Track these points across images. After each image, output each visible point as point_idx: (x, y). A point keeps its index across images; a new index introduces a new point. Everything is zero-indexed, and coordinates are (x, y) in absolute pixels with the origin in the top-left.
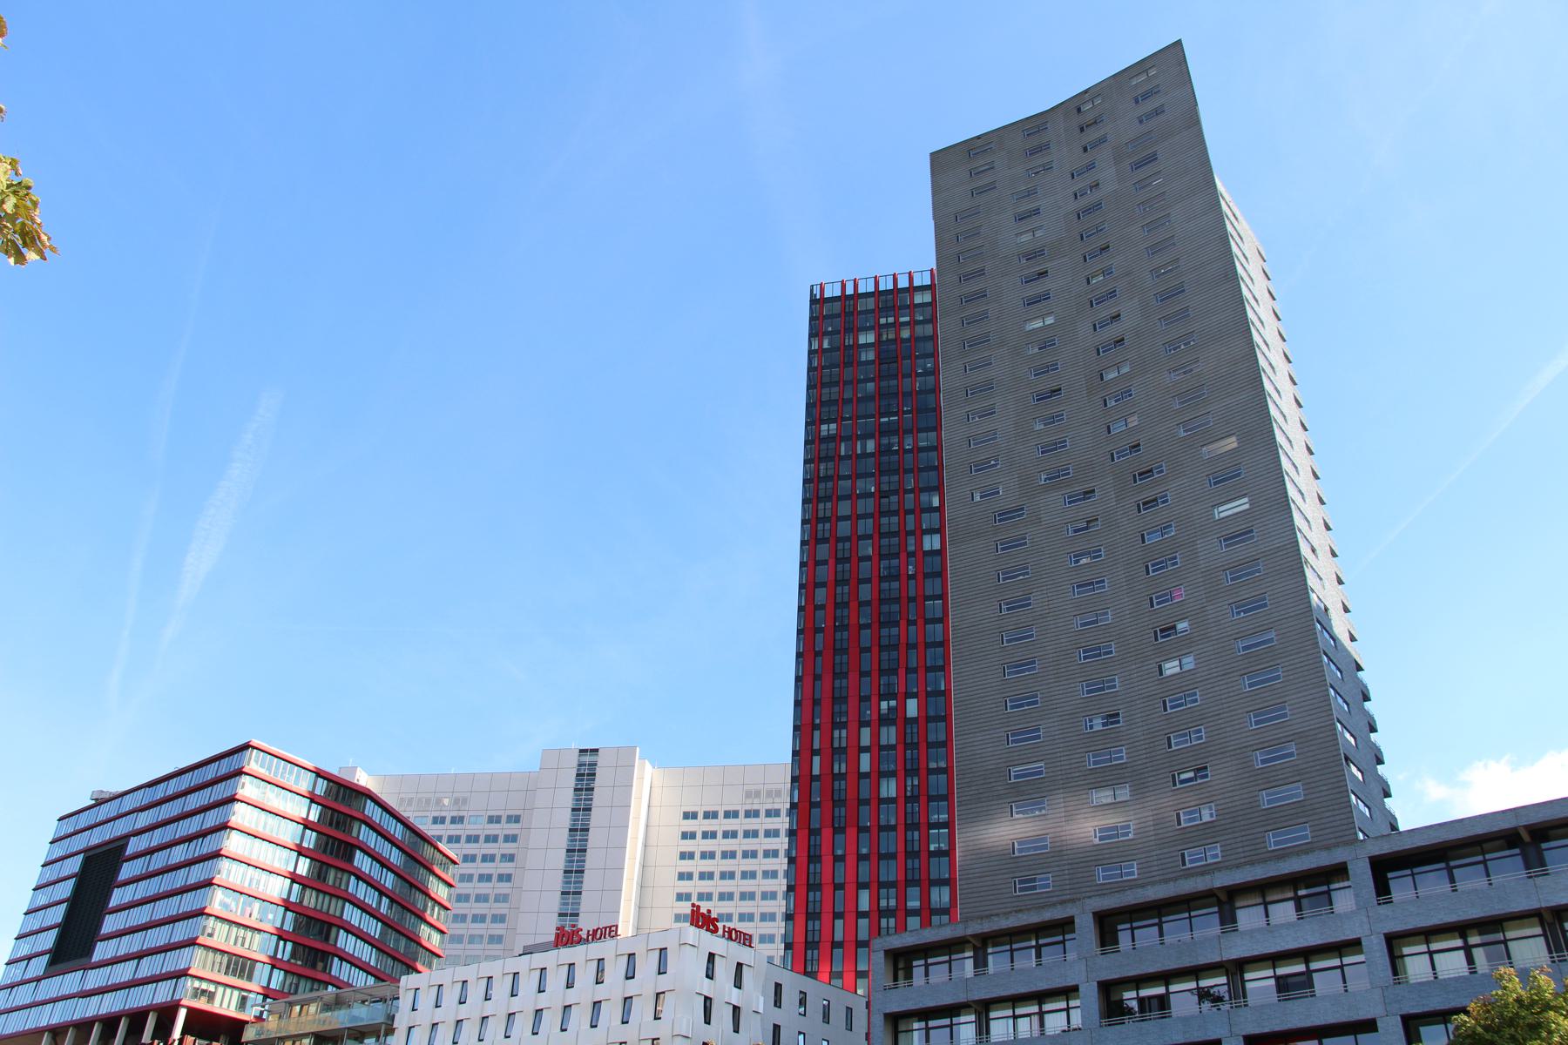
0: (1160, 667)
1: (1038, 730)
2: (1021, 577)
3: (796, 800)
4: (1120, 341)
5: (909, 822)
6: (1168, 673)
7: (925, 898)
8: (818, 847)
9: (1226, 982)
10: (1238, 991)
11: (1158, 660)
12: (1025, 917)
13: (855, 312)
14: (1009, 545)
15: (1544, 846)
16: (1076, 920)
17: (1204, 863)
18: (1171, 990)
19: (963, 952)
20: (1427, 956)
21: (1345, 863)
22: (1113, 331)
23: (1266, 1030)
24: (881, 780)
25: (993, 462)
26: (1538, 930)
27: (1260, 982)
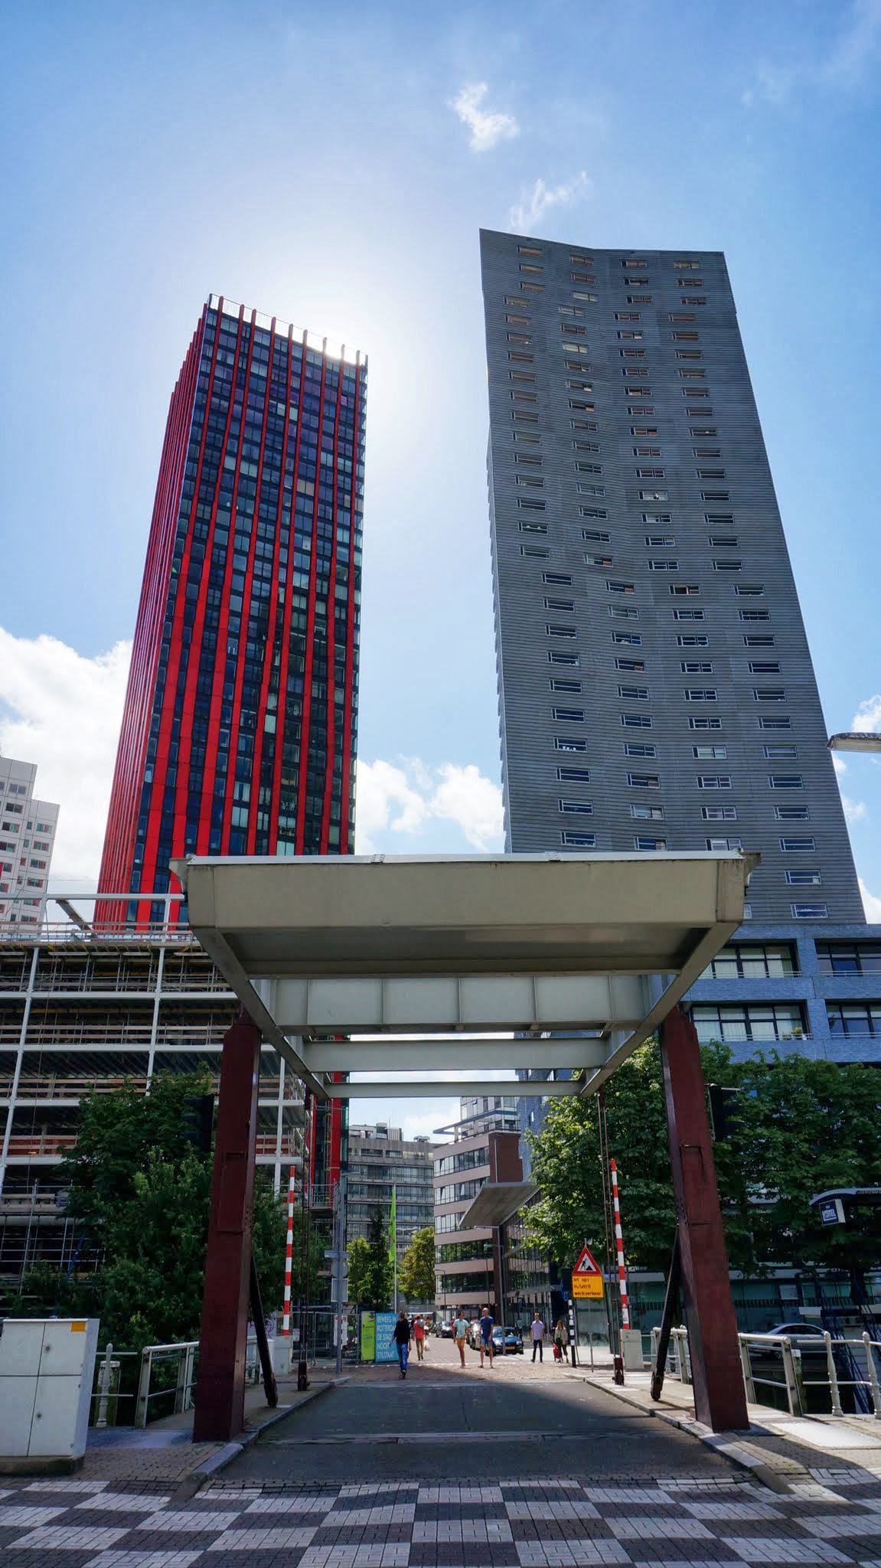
22: (650, 462)
25: (539, 528)
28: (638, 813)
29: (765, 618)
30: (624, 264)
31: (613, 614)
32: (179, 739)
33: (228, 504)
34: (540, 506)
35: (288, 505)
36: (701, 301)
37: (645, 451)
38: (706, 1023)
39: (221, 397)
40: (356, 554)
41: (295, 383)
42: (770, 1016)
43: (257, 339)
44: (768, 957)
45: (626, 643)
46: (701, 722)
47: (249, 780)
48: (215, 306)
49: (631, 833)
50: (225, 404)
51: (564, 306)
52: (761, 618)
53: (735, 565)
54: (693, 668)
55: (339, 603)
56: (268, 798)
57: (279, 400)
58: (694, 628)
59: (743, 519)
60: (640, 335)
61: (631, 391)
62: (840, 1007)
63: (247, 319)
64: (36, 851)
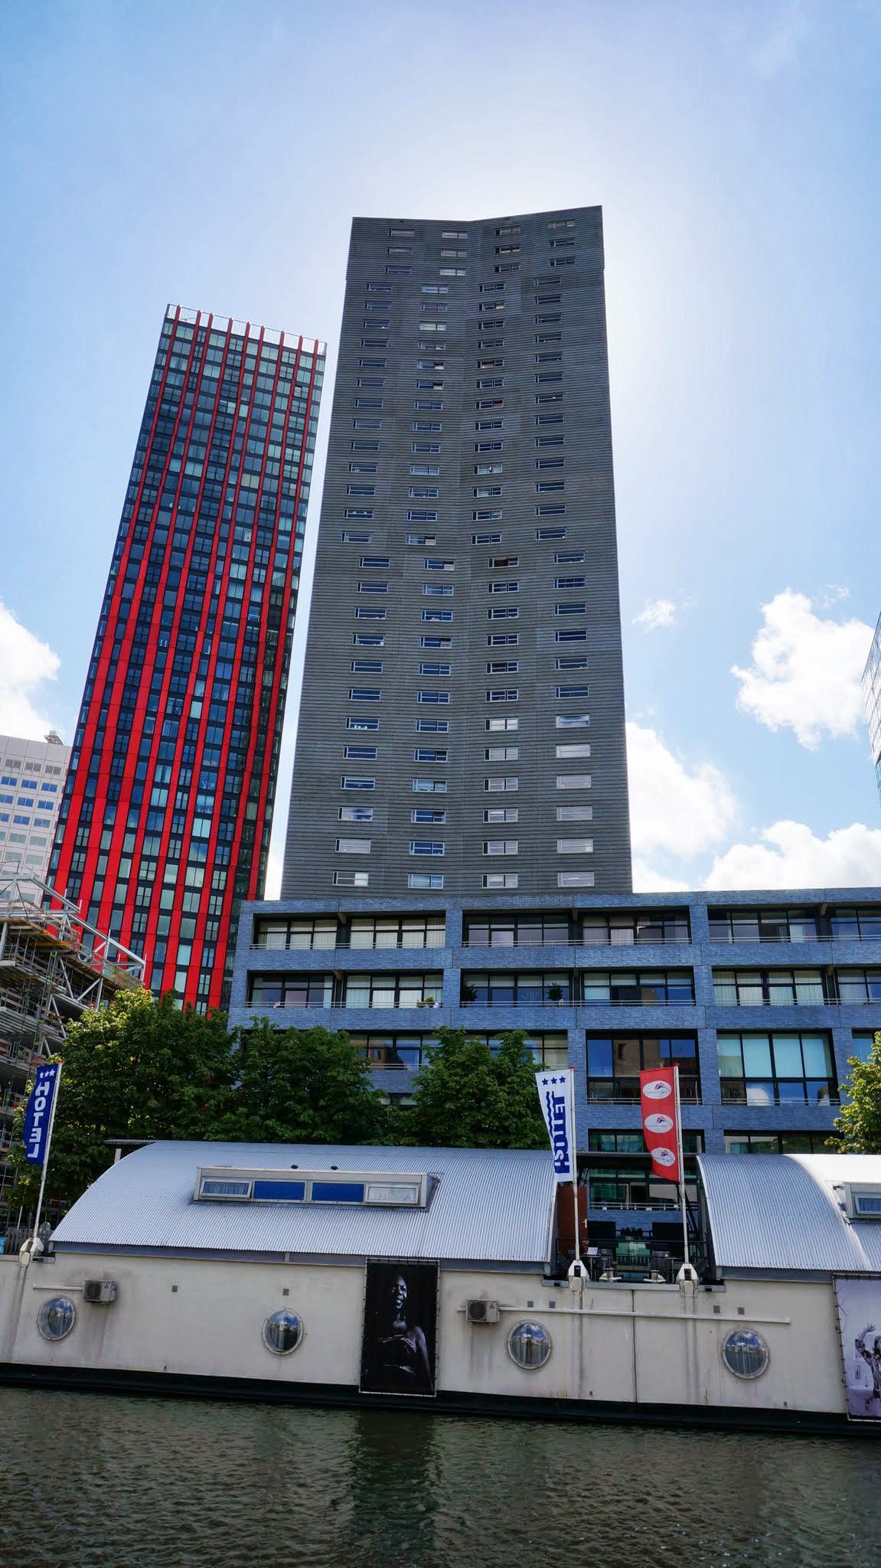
0: (488, 722)
1: (374, 751)
2: (377, 618)
3: (75, 767)
4: (498, 446)
5: (82, 819)
6: (493, 728)
7: (181, 875)
8: (89, 815)
9: (568, 985)
10: (577, 994)
11: (487, 716)
12: (399, 904)
13: (206, 345)
14: (370, 587)
15: (833, 920)
16: (447, 915)
17: (503, 887)
18: (519, 985)
19: (674, 920)
20: (734, 988)
21: (688, 907)
22: (491, 435)
23: (607, 1027)
24: (158, 766)
25: (365, 513)
26: (819, 980)
27: (597, 992)
28: (419, 786)
29: (581, 585)
30: (498, 233)
31: (427, 592)
32: (104, 729)
33: (171, 505)
34: (370, 490)
35: (231, 500)
36: (570, 261)
37: (486, 426)
38: (358, 991)
39: (171, 403)
40: (298, 542)
41: (248, 380)
42: (789, 981)
43: (214, 341)
44: (429, 927)
45: (437, 620)
46: (498, 695)
47: (170, 763)
48: (172, 316)
49: (410, 806)
50: (175, 409)
51: (428, 285)
52: (577, 585)
53: (560, 533)
54: (499, 640)
55: (275, 590)
56: (188, 779)
57: (229, 399)
58: (506, 599)
59: (574, 485)
60: (502, 304)
61: (483, 364)
62: (865, 972)
63: (204, 323)
64: (37, 828)
